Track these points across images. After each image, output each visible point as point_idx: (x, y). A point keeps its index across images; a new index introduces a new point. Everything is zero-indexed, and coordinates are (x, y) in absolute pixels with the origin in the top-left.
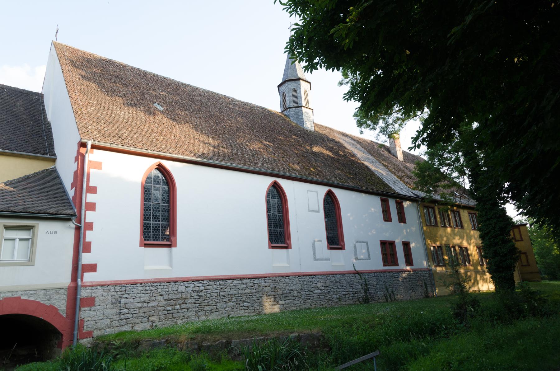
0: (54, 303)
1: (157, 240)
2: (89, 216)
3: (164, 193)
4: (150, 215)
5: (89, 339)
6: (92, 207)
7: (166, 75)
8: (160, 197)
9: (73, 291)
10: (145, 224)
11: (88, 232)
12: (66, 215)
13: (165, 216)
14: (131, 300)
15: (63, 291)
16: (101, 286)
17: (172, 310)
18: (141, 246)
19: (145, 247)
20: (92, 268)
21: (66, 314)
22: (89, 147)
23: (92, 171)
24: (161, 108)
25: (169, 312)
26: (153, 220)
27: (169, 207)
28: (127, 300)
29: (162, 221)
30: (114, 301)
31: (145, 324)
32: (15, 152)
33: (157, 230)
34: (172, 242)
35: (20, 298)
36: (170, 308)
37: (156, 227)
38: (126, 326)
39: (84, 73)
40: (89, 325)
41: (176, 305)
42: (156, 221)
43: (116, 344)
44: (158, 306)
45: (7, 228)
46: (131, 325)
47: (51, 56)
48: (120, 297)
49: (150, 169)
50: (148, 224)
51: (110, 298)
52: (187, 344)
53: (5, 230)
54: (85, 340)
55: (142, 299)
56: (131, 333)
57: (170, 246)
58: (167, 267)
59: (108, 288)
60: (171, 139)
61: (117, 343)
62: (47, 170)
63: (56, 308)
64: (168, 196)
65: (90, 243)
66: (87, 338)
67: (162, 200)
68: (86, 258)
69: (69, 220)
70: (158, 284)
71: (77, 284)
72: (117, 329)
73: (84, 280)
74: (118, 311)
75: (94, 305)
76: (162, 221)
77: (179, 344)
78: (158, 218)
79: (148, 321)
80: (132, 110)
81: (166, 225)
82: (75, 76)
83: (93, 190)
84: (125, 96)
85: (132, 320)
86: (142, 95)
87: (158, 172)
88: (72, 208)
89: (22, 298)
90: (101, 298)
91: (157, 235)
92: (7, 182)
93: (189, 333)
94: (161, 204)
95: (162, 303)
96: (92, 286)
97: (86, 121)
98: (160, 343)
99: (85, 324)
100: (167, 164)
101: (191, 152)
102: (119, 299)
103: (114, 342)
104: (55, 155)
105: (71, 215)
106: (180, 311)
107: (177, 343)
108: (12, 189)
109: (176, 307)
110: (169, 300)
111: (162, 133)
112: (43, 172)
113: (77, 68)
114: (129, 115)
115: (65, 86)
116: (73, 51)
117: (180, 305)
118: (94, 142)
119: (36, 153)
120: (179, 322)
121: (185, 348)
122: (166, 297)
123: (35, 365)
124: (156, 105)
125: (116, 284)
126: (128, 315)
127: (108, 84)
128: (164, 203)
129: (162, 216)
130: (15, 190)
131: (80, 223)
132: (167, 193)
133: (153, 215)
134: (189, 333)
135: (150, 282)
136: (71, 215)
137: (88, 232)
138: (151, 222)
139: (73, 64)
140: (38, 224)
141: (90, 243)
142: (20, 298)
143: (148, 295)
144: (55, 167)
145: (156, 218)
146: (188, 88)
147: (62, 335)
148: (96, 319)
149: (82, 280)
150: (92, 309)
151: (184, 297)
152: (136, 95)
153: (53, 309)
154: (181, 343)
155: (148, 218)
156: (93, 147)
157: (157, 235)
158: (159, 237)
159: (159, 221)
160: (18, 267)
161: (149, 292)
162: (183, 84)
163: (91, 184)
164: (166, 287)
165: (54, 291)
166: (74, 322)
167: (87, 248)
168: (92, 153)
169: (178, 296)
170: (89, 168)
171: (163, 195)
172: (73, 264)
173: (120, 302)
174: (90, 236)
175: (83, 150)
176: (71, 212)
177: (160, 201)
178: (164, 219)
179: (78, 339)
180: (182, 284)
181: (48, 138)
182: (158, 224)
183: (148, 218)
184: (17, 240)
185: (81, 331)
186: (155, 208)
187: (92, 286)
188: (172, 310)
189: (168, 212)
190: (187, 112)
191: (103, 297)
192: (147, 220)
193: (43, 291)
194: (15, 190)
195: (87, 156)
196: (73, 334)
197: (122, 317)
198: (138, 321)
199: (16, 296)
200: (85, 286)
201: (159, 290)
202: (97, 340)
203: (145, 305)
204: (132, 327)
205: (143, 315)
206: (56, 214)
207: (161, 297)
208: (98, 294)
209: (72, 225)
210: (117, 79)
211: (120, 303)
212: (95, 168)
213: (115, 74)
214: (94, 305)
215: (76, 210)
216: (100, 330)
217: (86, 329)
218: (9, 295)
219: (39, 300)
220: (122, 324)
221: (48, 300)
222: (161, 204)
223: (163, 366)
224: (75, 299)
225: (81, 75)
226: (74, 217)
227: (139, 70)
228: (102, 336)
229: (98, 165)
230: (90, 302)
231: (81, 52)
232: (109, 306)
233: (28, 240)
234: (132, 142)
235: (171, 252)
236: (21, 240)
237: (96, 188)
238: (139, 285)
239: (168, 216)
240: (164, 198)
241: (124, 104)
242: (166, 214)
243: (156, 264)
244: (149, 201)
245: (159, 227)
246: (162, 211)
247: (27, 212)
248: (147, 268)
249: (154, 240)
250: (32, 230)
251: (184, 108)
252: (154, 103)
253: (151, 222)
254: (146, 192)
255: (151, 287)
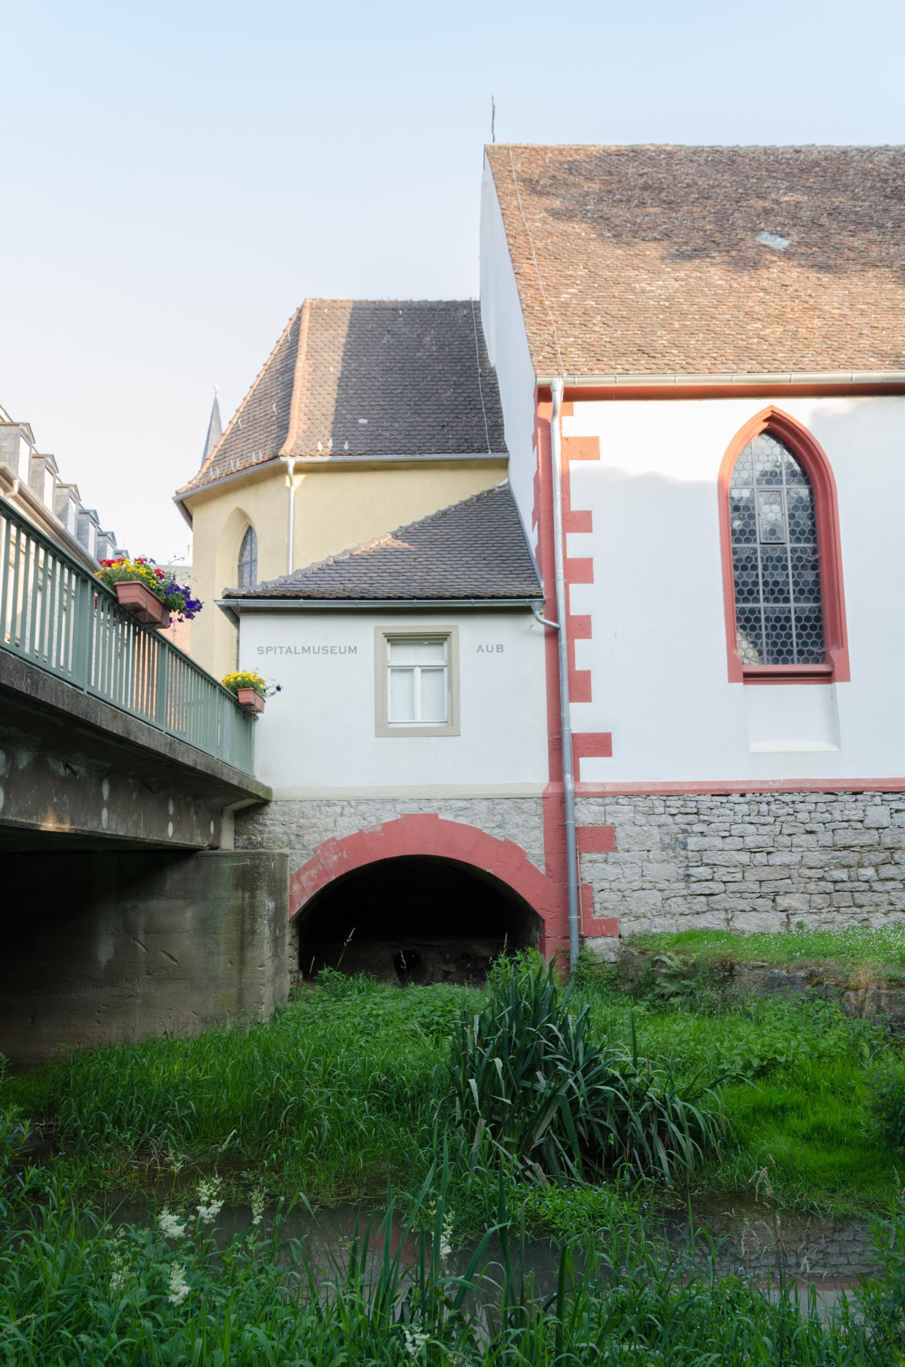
0: (513, 836)
1: (785, 662)
2: (579, 599)
3: (796, 508)
4: (756, 584)
5: (609, 940)
6: (582, 571)
7: (799, 141)
8: (785, 525)
9: (557, 806)
10: (742, 611)
11: (580, 644)
12: (519, 597)
13: (806, 583)
14: (718, 842)
15: (532, 805)
16: (627, 795)
17: (850, 879)
18: (732, 679)
19: (745, 682)
20: (600, 745)
21: (547, 865)
22: (558, 396)
23: (575, 465)
24: (781, 243)
25: (839, 886)
26: (766, 600)
27: (815, 551)
28: (704, 842)
29: (797, 600)
30: (667, 839)
31: (764, 915)
32: (417, 457)
33: (783, 628)
34: (832, 665)
35: (435, 816)
36: (843, 874)
37: (778, 619)
38: (709, 915)
39: (557, 203)
40: (606, 904)
41: (861, 865)
42: (776, 600)
43: (669, 962)
44: (801, 864)
45: (394, 640)
46: (722, 915)
47: (484, 185)
48: (684, 831)
49: (743, 439)
50: (752, 611)
51: (655, 831)
52: (876, 997)
53: (389, 646)
54: (600, 941)
55: (750, 842)
56: (718, 935)
57: (827, 677)
58: (823, 745)
59: (648, 803)
60: (810, 330)
61: (674, 962)
62: (490, 492)
63: (520, 850)
64: (812, 517)
65: (587, 674)
66: (604, 935)
67: (792, 532)
68: (580, 718)
69: (527, 611)
70: (797, 798)
71: (563, 787)
72: (682, 920)
73: (583, 779)
74: (681, 871)
75: (615, 849)
76: (797, 600)
77: (851, 994)
78: (781, 592)
79: (774, 908)
80: (685, 270)
81: (811, 610)
82: (535, 215)
83: (581, 522)
84: (667, 235)
85: (723, 900)
86: (722, 218)
87: (773, 442)
88: (536, 581)
89: (441, 817)
90: (629, 829)
91: (784, 644)
92: (398, 531)
93: (889, 961)
94: (789, 546)
95: (815, 858)
96: (602, 795)
97: (552, 328)
98: (791, 981)
99: (596, 899)
100: (799, 411)
101: (882, 355)
102: (680, 836)
103: (664, 959)
104: (505, 450)
105: (531, 597)
106: (877, 886)
107: (844, 988)
108: (406, 545)
109: (862, 871)
110: (835, 848)
111: (780, 318)
112: (479, 498)
113: (540, 194)
114: (677, 285)
115: (506, 248)
116: (533, 153)
117: (876, 866)
118: (571, 379)
119: (463, 452)
120: (878, 921)
121: (869, 1007)
122: (826, 838)
123: (448, 987)
124: (765, 239)
125: (668, 793)
126: (710, 884)
127: (620, 214)
128: (798, 540)
129: (796, 583)
130: (412, 548)
131: (556, 619)
132: (805, 509)
133: (766, 584)
134: (889, 961)
135: (771, 791)
136: (531, 597)
137: (579, 643)
138: (762, 605)
139: (532, 186)
140: (457, 627)
141: (587, 674)
142: (435, 816)
143: (768, 828)
144: (508, 484)
145: (777, 592)
146: (881, 157)
147: (544, 921)
148: (623, 887)
149: (576, 777)
150: (611, 860)
151: (888, 841)
152: (700, 223)
153: (511, 849)
154: (856, 990)
155: (751, 592)
156: (571, 395)
157: (784, 644)
158: (790, 652)
159: (787, 600)
160: (424, 740)
161: (771, 820)
162: (861, 151)
163: (575, 506)
164: (822, 807)
165: (510, 802)
166: (566, 891)
167: (582, 688)
168: (571, 413)
169: (865, 839)
170: (565, 460)
171: (792, 516)
172: (550, 733)
173: (685, 847)
174: (584, 654)
175: (545, 409)
176: (532, 590)
177: (786, 536)
178: (801, 592)
179: (581, 936)
180: (878, 800)
181: (489, 410)
182: (782, 610)
183: (751, 592)
184: (418, 671)
185: (588, 915)
186: (770, 559)
187: (607, 795)
188: (850, 879)
189: (814, 568)
190: (873, 234)
191: (637, 828)
192: (746, 600)
193: (485, 803)
194: (412, 548)
195: (556, 424)
196: (567, 922)
197: (696, 888)
198: (743, 905)
199: (427, 811)
200: (587, 795)
201: (803, 816)
202: (631, 944)
203: (761, 858)
204: (728, 921)
205: (755, 887)
206: (493, 597)
207: (810, 837)
208: (622, 818)
209: (537, 624)
210: (646, 194)
211: (685, 849)
212: (583, 456)
213: (641, 181)
214: (615, 849)
215: (543, 584)
216: (637, 918)
217: (598, 913)
218: (413, 808)
219: (478, 825)
220: (698, 908)
221: (499, 827)
222: (789, 546)
223: (782, 1059)
224: (563, 827)
225: (547, 210)
226: (536, 604)
227: (715, 151)
228: (646, 937)
229: (588, 448)
230: (603, 839)
231: (552, 150)
232: (656, 854)
233: (439, 670)
234: (680, 360)
235: (833, 697)
236: (426, 670)
237: (588, 515)
238: (735, 798)
239: (816, 583)
240: (797, 524)
241: (663, 259)
242: (809, 576)
243: (786, 736)
244: (748, 540)
245: (788, 619)
246: (795, 567)
247: (427, 598)
248: (757, 746)
249: (776, 662)
250: (446, 644)
251: (861, 224)
252: (755, 231)
253: (762, 605)
254: (739, 518)
255: (773, 807)
